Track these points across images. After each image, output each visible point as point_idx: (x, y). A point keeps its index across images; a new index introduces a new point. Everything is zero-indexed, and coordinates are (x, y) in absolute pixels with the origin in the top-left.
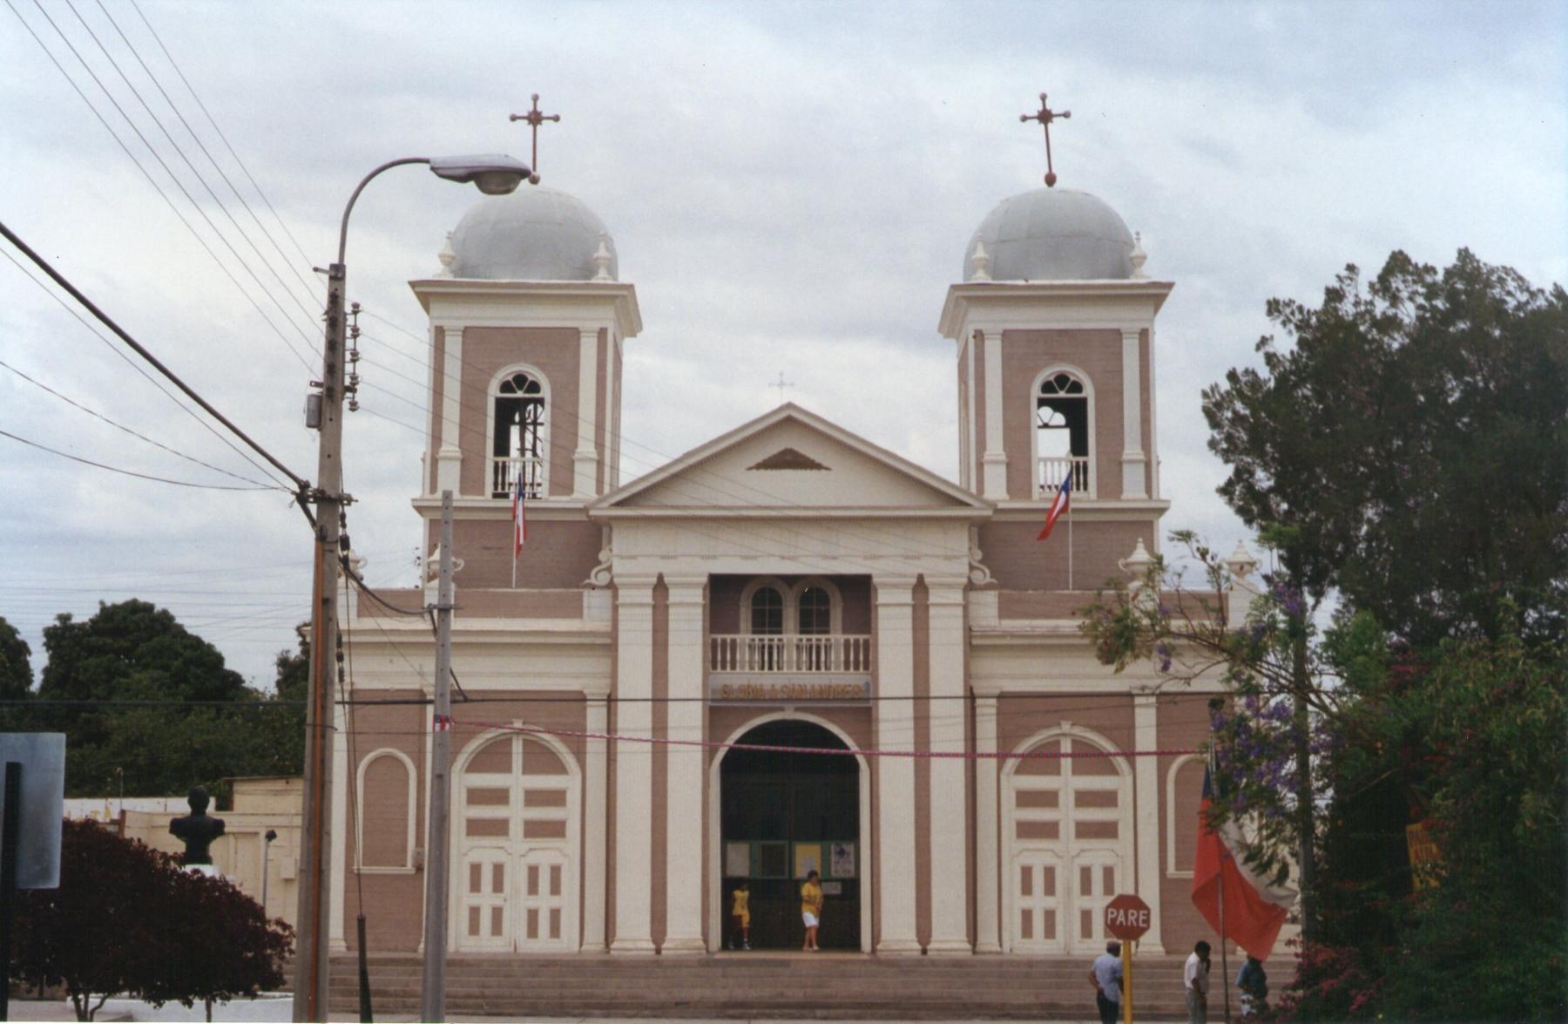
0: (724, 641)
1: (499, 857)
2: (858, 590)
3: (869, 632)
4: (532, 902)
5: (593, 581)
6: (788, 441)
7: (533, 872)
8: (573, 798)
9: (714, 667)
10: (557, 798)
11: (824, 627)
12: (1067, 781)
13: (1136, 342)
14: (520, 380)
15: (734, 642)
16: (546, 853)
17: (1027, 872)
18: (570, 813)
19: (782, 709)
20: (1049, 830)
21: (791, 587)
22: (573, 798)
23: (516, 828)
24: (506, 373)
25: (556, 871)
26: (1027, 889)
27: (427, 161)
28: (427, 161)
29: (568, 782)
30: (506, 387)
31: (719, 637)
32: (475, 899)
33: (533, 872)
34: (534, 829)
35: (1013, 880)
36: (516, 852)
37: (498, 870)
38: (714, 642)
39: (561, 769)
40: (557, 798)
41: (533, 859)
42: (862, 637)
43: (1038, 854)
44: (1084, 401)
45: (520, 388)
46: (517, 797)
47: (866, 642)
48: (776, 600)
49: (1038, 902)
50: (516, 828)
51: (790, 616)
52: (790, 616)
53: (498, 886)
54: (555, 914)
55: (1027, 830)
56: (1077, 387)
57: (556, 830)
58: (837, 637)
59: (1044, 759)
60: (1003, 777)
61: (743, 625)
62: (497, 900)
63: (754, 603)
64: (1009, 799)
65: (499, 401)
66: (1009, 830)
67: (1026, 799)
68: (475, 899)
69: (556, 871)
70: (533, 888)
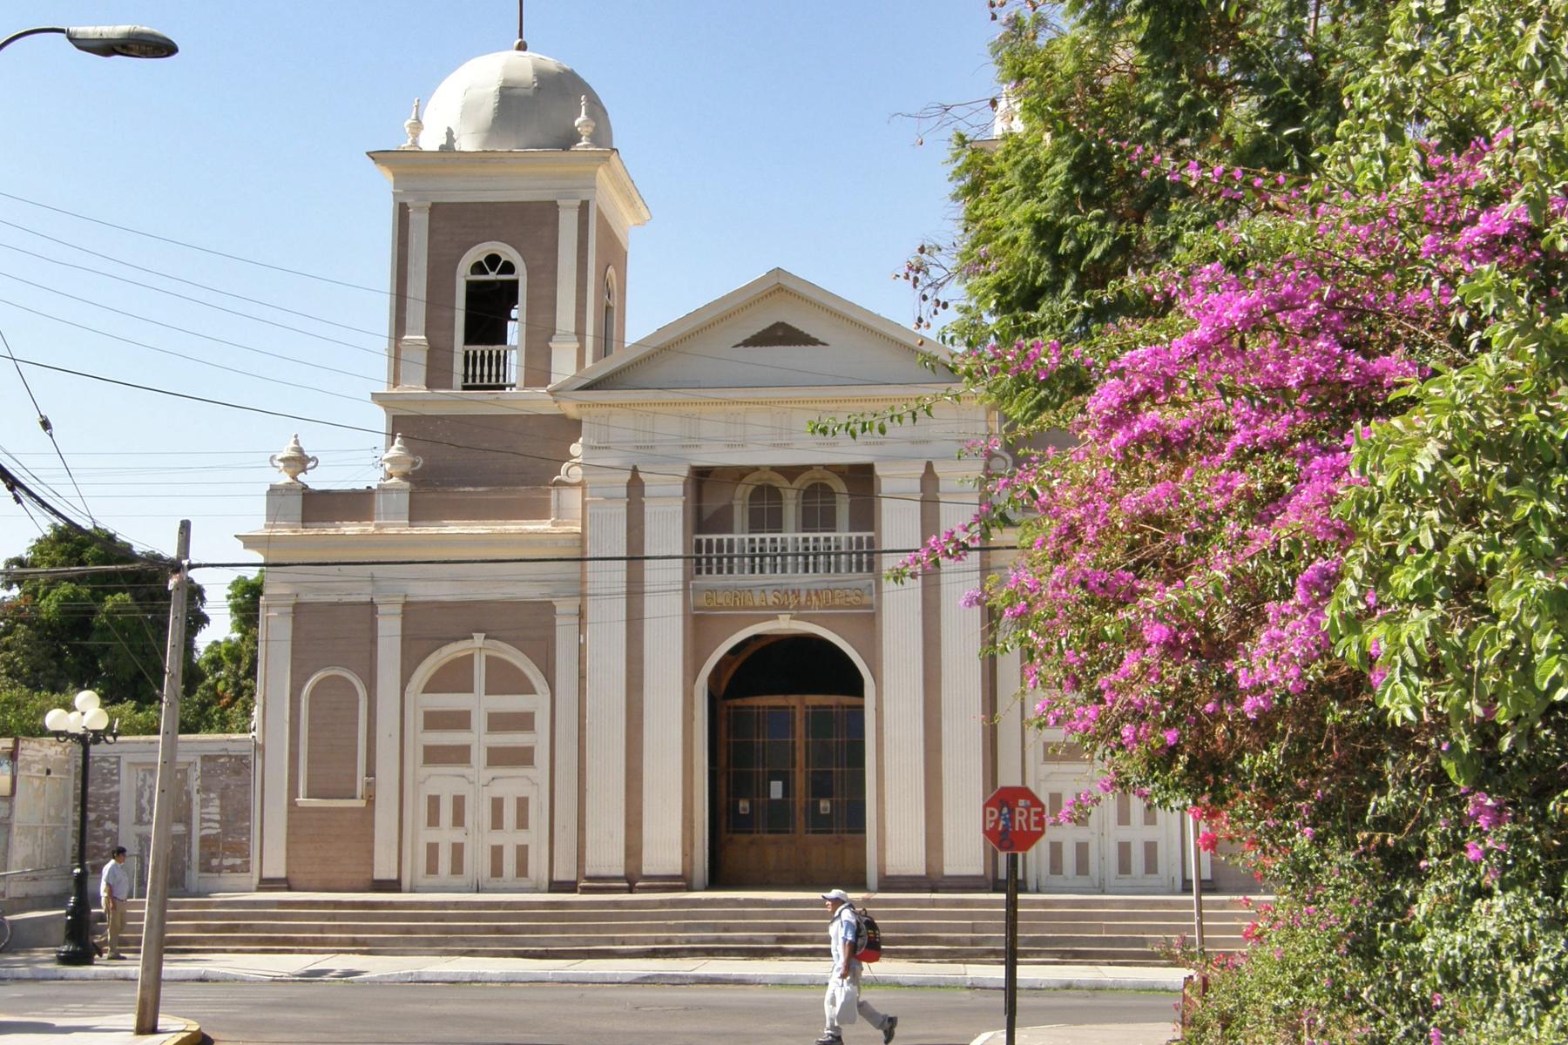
0: (720, 541)
1: (460, 787)
2: (861, 478)
3: (871, 529)
4: (497, 838)
5: (562, 477)
6: (778, 323)
7: (497, 804)
8: (542, 722)
9: (699, 571)
10: (523, 721)
11: (829, 524)
12: (479, 703)
13: (575, 214)
14: (493, 260)
15: (731, 541)
16: (511, 784)
17: (434, 802)
18: (538, 739)
19: (775, 617)
20: (460, 755)
21: (791, 480)
22: (542, 722)
23: (479, 756)
24: (478, 253)
25: (522, 804)
26: (433, 820)
27: (62, 31)
28: (62, 31)
29: (537, 703)
30: (478, 268)
31: (704, 538)
32: (432, 835)
33: (497, 804)
34: (497, 757)
35: (417, 811)
36: (477, 782)
37: (459, 802)
38: (699, 542)
39: (531, 690)
40: (523, 721)
41: (497, 790)
42: (865, 535)
43: (444, 782)
44: (514, 284)
45: (493, 269)
46: (479, 721)
47: (870, 540)
48: (774, 494)
49: (446, 835)
50: (479, 756)
51: (791, 510)
52: (791, 510)
53: (458, 820)
54: (522, 851)
55: (434, 755)
56: (509, 268)
57: (523, 757)
58: (843, 535)
59: (454, 678)
60: (409, 697)
61: (737, 525)
62: (457, 836)
63: (752, 497)
64: (415, 720)
65: (470, 284)
66: (414, 755)
67: (434, 721)
68: (432, 835)
69: (522, 804)
70: (497, 823)
